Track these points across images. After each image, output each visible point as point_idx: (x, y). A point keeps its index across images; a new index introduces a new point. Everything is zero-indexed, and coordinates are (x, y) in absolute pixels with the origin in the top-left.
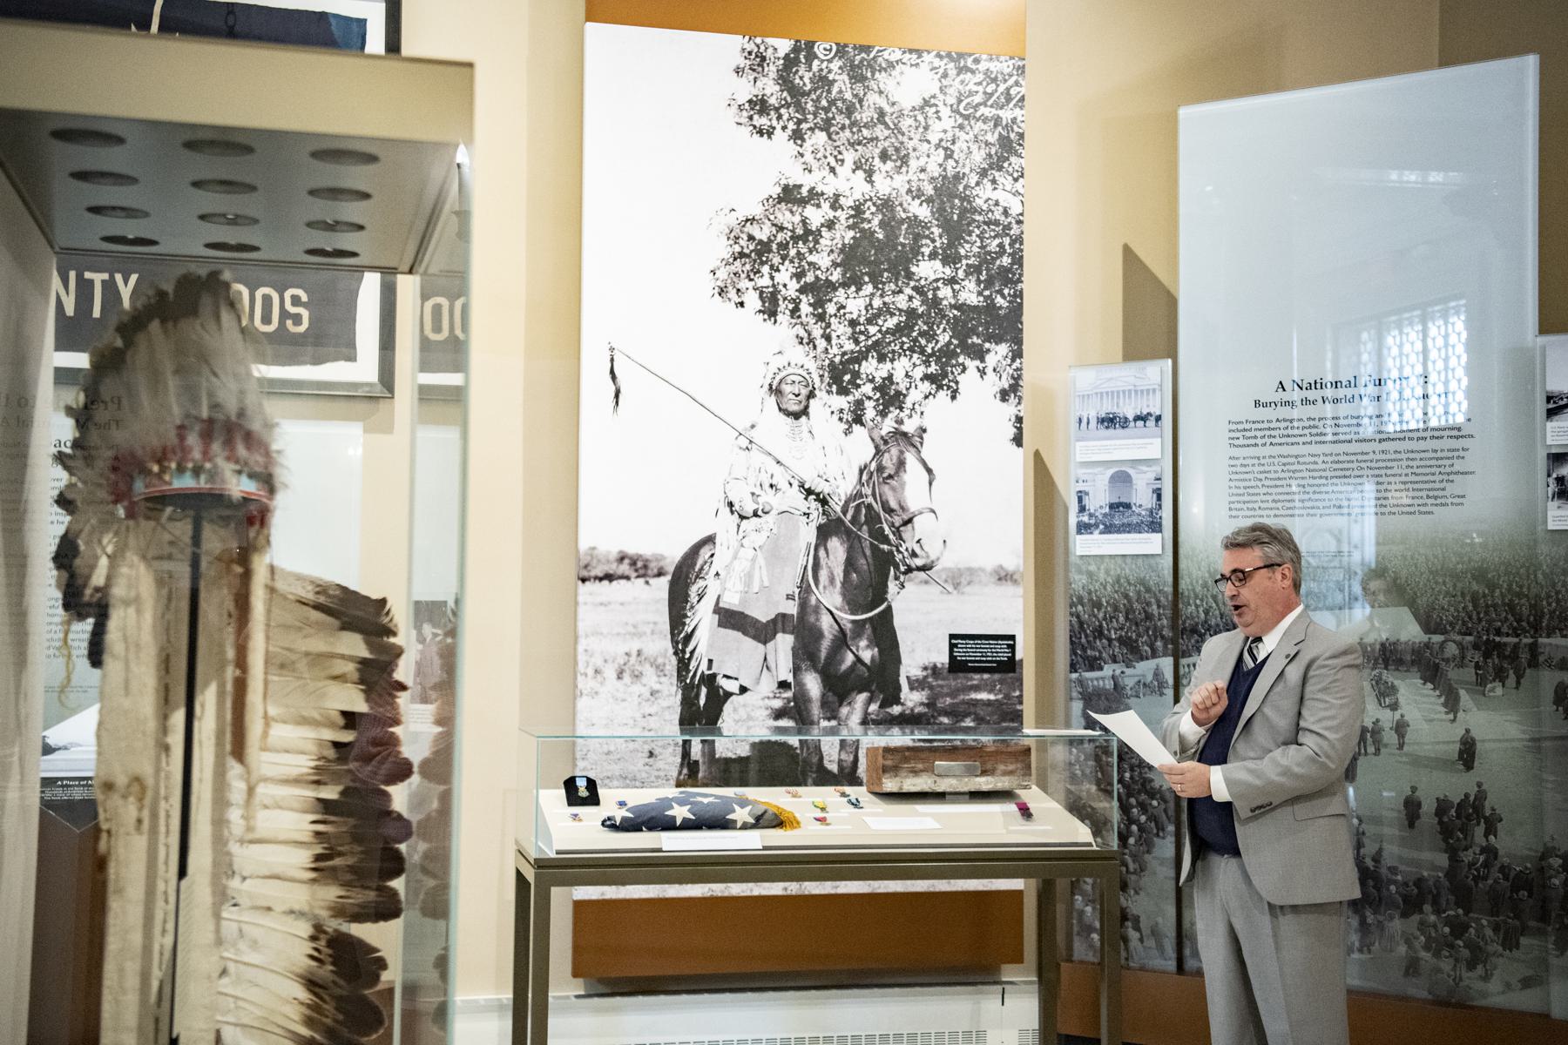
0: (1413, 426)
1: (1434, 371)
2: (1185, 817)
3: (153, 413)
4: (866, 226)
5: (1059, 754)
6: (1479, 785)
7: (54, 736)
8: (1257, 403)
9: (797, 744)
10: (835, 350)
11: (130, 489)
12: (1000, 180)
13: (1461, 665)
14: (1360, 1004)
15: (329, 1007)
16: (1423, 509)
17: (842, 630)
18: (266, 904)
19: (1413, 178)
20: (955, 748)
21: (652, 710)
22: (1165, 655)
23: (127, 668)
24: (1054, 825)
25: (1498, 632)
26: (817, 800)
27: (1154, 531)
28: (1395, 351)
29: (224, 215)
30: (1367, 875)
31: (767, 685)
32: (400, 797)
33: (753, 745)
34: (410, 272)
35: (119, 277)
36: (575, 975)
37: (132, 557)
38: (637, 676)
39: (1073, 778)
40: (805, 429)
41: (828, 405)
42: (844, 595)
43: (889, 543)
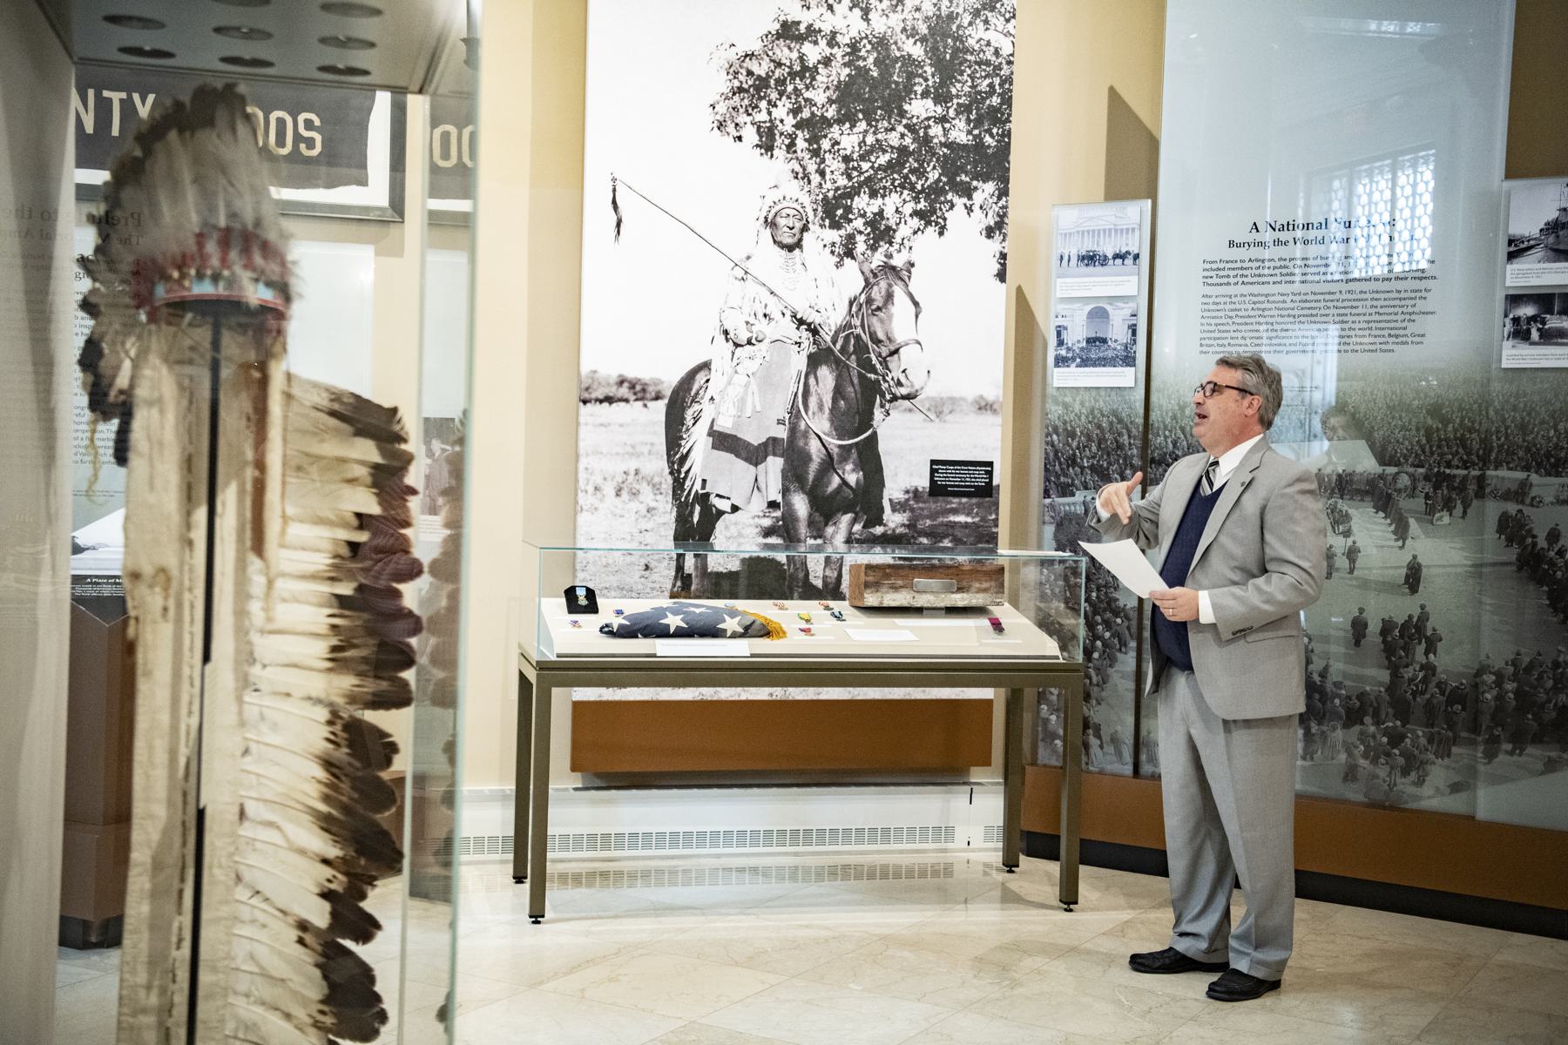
0: (1378, 272)
1: (1402, 216)
2: (1147, 634)
3: (177, 216)
4: (861, 63)
5: (1031, 574)
6: (1423, 607)
7: (83, 536)
8: (1231, 244)
9: (784, 560)
10: (829, 185)
11: (151, 293)
12: (993, 20)
13: (1412, 496)
14: (1305, 807)
15: (345, 786)
16: (1384, 347)
17: (829, 454)
19: (1392, 28)
20: (933, 567)
21: (648, 526)
24: (1025, 639)
25: (1449, 465)
26: (804, 613)
28: (1364, 199)
29: (238, 29)
30: (1315, 690)
32: (412, 594)
33: (743, 561)
34: (420, 92)
35: (136, 97)
36: (574, 769)
37: (154, 359)
38: (635, 494)
39: (1043, 597)
40: (798, 261)
41: (820, 238)
42: (832, 422)
43: (876, 373)
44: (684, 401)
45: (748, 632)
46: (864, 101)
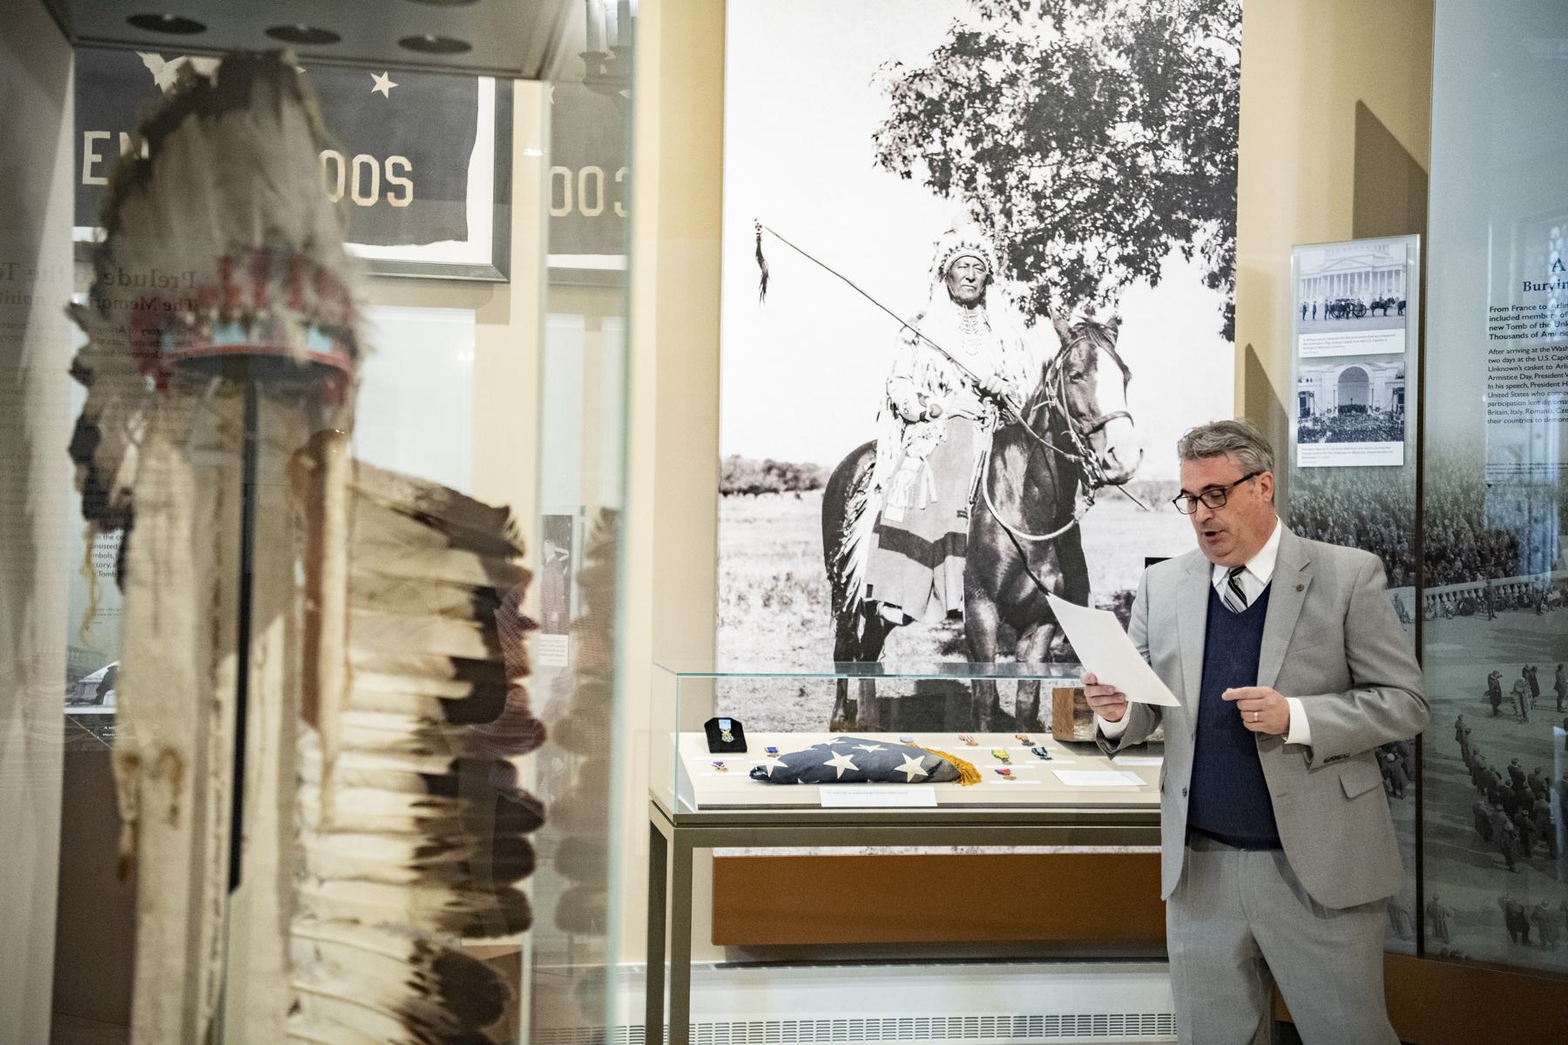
3: (188, 247)
4: (1054, 81)
12: (1214, 25)
18: (349, 914)
21: (803, 643)
22: (1405, 584)
23: (157, 598)
26: (998, 749)
27: (1394, 439)
31: (935, 615)
33: (919, 684)
34: (538, 76)
37: (161, 444)
38: (786, 604)
40: (980, 319)
41: (1006, 292)
43: (1076, 452)
44: (844, 490)
45: (934, 774)
46: (1057, 126)
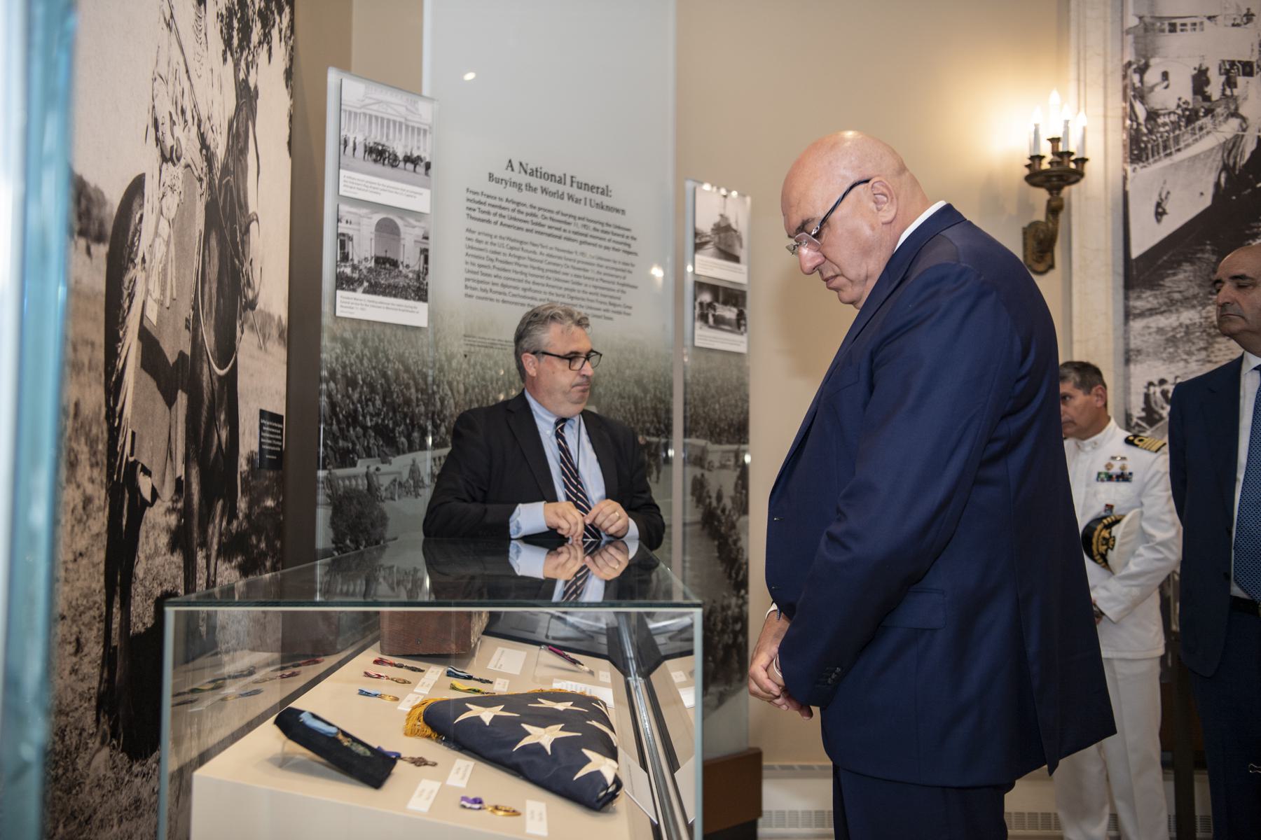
8: (491, 176)
